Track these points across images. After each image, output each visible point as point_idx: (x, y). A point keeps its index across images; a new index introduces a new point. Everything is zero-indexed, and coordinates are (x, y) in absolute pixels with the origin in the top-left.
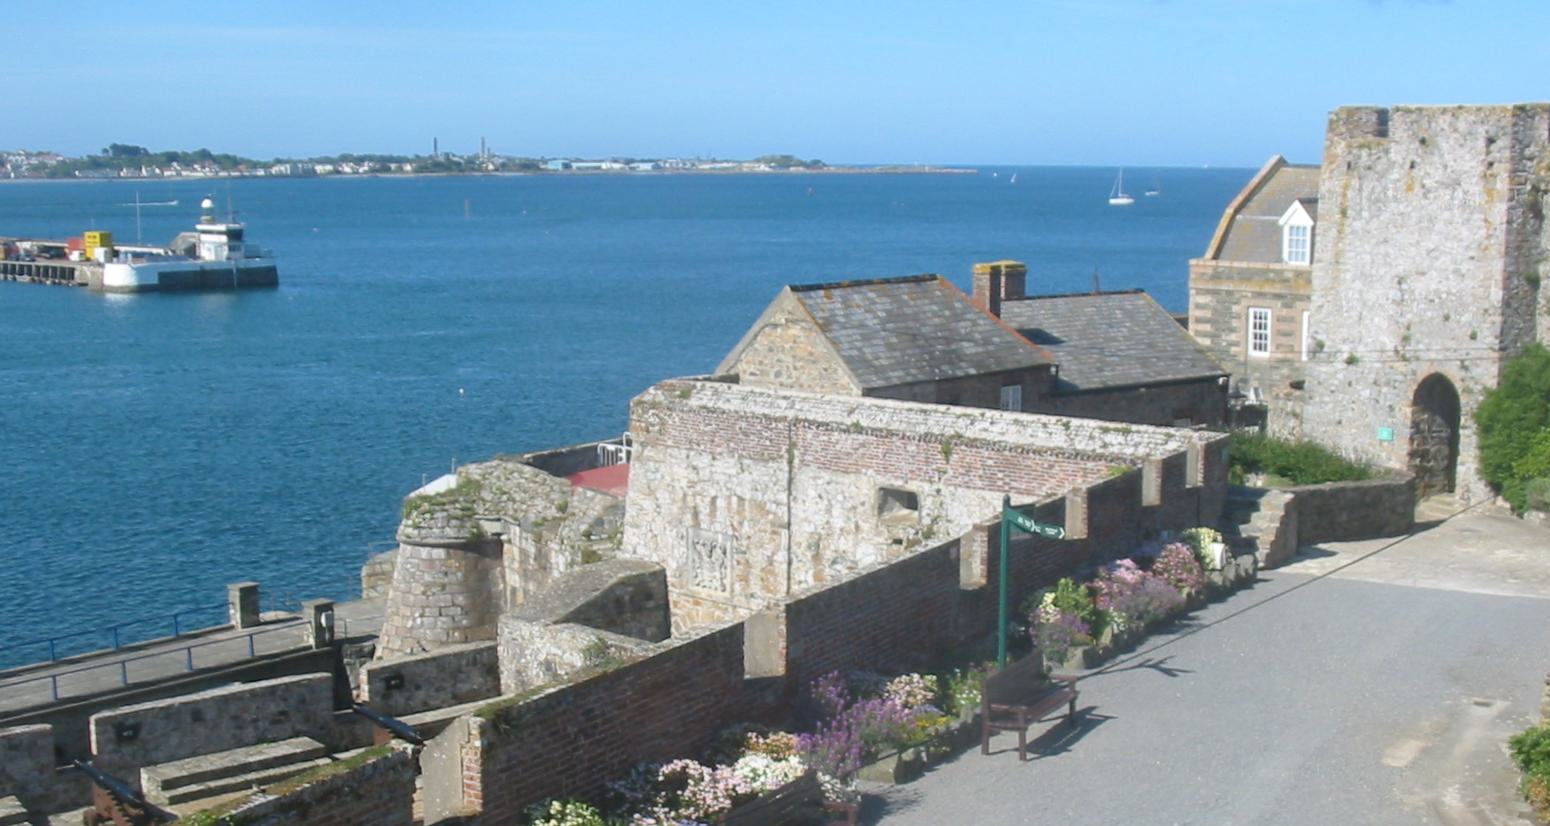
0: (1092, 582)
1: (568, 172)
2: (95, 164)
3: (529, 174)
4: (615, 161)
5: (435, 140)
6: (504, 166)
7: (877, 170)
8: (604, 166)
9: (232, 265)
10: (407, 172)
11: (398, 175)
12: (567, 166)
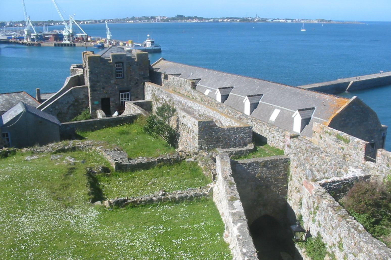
0: (376, 220)
2: (173, 19)
4: (284, 20)
6: (259, 20)
9: (151, 48)
12: (272, 21)
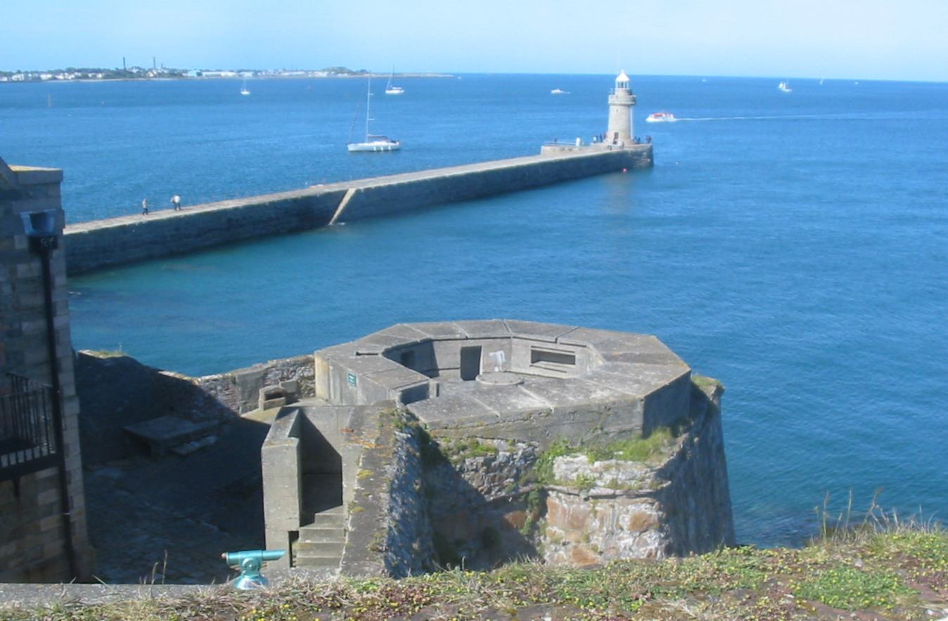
1: (199, 78)
3: (175, 79)
4: (232, 71)
5: (124, 59)
7: (405, 76)
8: (223, 74)
10: (99, 78)
11: (92, 81)
12: (199, 74)
